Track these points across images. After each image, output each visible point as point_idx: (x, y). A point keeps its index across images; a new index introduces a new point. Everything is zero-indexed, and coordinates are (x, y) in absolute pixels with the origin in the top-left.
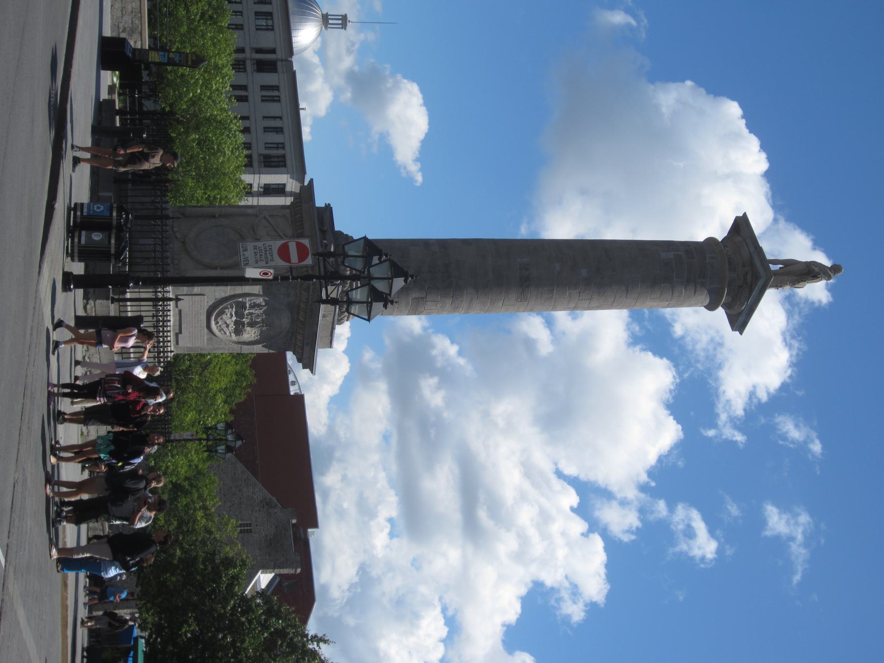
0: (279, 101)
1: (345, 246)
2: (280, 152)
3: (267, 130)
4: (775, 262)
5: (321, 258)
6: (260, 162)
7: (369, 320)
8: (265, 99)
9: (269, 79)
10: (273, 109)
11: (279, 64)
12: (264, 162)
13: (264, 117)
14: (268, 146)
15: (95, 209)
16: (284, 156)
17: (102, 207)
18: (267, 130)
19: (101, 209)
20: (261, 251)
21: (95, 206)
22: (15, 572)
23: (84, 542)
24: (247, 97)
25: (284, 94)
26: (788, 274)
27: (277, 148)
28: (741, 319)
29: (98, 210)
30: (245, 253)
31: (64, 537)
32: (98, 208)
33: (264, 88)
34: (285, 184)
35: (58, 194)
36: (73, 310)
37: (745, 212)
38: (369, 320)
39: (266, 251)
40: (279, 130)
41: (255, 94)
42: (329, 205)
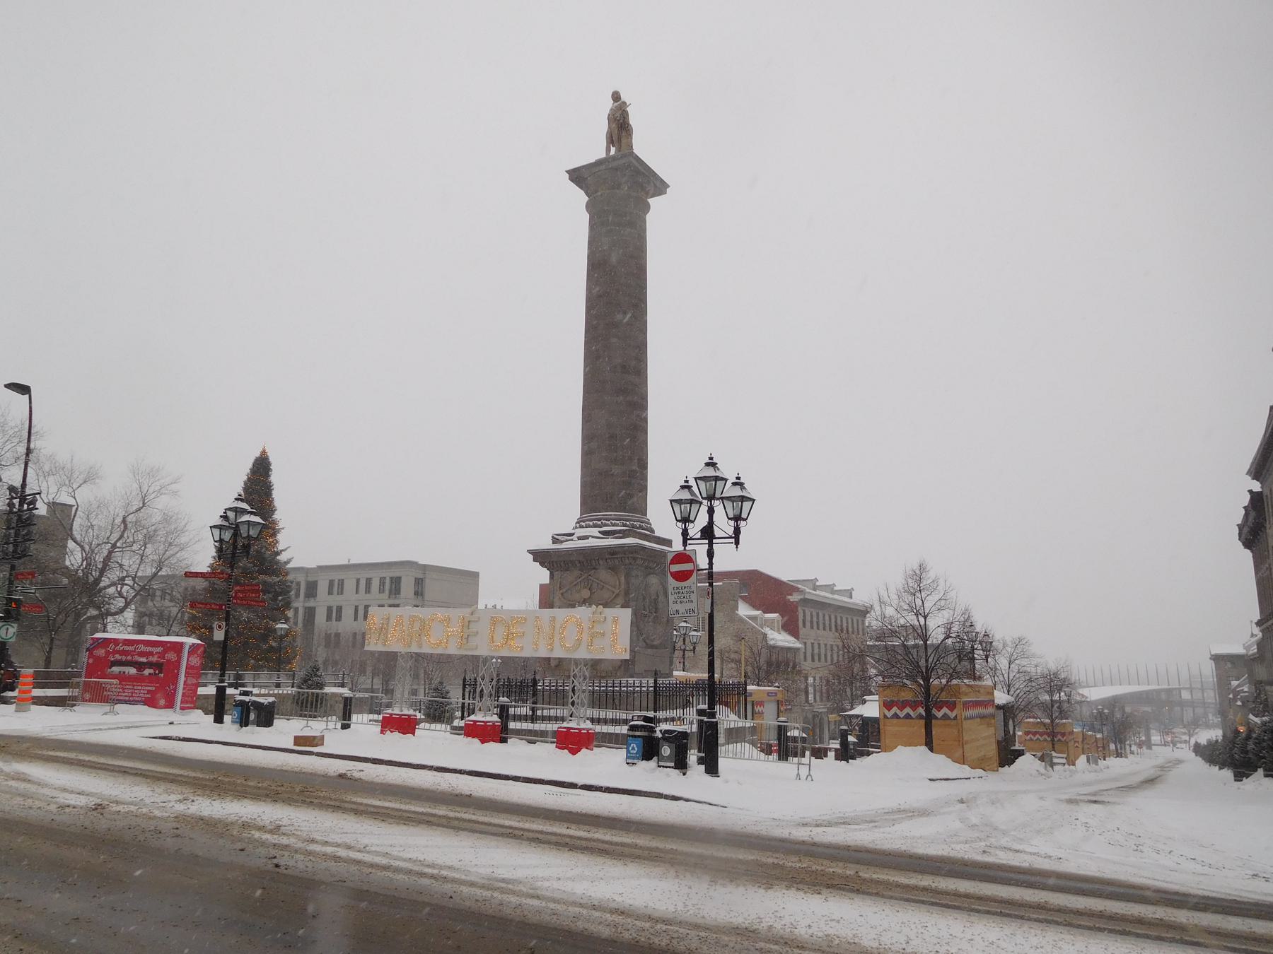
0: (343, 580)
1: (730, 517)
2: (388, 581)
3: (368, 590)
4: (608, 150)
5: (689, 542)
6: (396, 597)
7: (754, 500)
8: (341, 592)
9: (322, 588)
10: (349, 586)
11: (310, 579)
12: (395, 594)
13: (357, 593)
14: (382, 590)
15: (635, 752)
16: (392, 578)
17: (632, 745)
18: (368, 590)
19: (635, 746)
20: (679, 598)
21: (632, 752)
22: (954, 895)
23: (707, 541)
24: (337, 607)
25: (336, 576)
26: (620, 140)
27: (384, 583)
28: (658, 184)
29: (636, 749)
30: (680, 612)
31: (156, 772)
32: (633, 749)
33: (330, 592)
34: (415, 578)
35: (205, 758)
36: (338, 761)
37: (566, 171)
38: (754, 500)
39: (679, 593)
40: (369, 581)
41: (335, 600)
42: (29, 387)
